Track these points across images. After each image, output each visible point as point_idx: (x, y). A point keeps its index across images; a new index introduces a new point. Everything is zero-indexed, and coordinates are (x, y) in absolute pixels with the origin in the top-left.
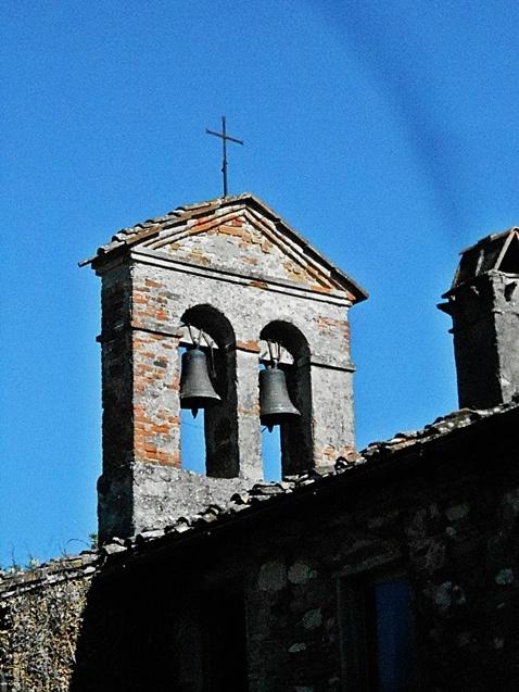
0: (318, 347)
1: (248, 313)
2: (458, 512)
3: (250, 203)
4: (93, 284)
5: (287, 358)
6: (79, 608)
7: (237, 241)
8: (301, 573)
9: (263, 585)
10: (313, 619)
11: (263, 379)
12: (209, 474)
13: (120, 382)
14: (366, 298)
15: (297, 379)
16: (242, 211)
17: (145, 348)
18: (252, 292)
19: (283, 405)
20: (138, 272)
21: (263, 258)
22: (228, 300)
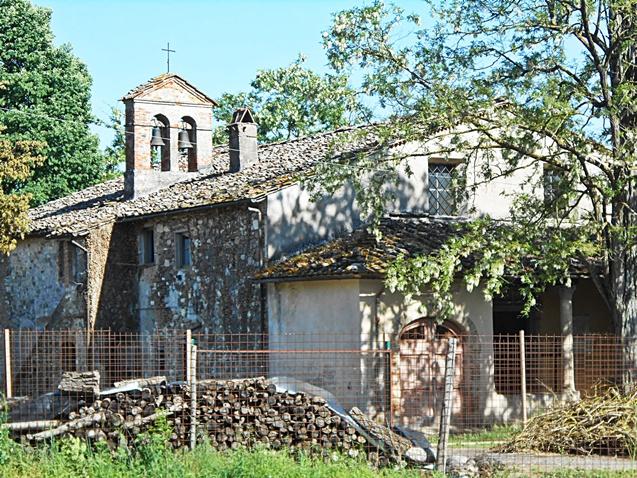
0: (199, 124)
1: (175, 118)
2: (200, 222)
3: (176, 76)
4: (123, 107)
5: (189, 127)
6: (110, 232)
7: (171, 90)
8: (167, 229)
9: (158, 230)
10: (169, 242)
11: (180, 135)
12: (163, 170)
13: (130, 142)
14: (156, 116)
15: (192, 135)
16: (173, 79)
17: (138, 132)
18: (177, 107)
19: (187, 144)
20: (136, 106)
21: (182, 95)
22: (166, 111)
